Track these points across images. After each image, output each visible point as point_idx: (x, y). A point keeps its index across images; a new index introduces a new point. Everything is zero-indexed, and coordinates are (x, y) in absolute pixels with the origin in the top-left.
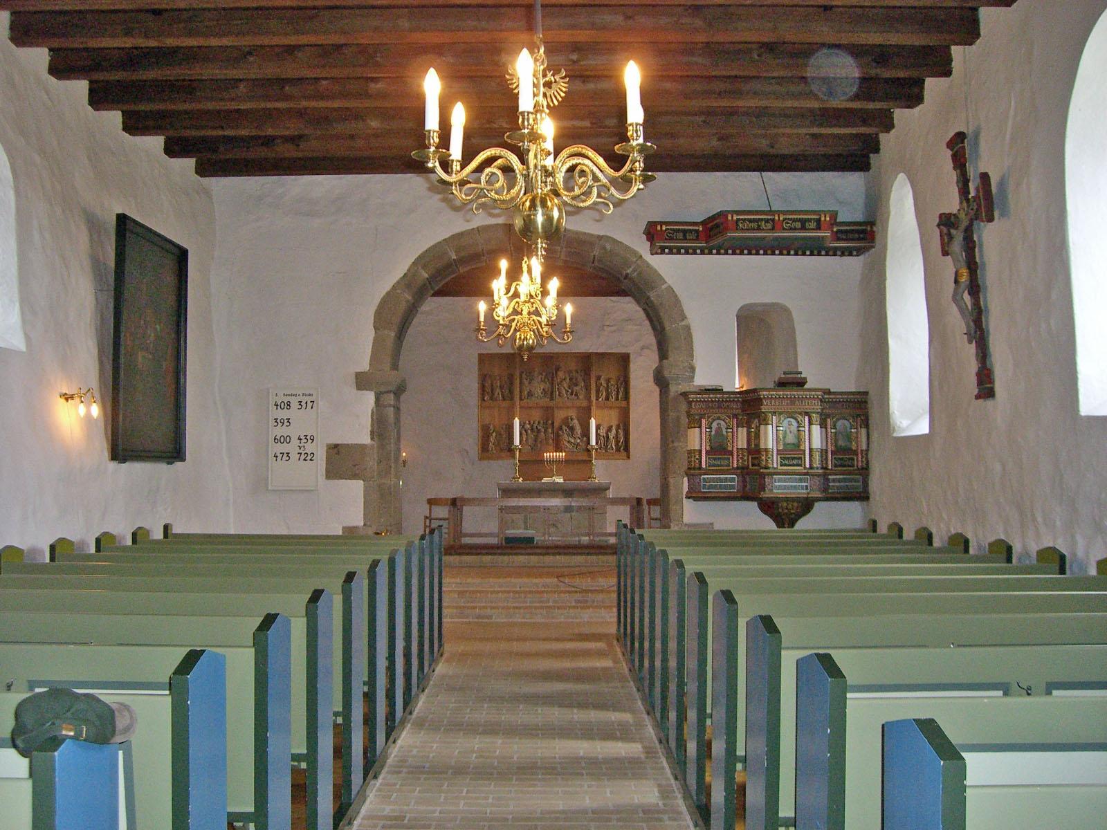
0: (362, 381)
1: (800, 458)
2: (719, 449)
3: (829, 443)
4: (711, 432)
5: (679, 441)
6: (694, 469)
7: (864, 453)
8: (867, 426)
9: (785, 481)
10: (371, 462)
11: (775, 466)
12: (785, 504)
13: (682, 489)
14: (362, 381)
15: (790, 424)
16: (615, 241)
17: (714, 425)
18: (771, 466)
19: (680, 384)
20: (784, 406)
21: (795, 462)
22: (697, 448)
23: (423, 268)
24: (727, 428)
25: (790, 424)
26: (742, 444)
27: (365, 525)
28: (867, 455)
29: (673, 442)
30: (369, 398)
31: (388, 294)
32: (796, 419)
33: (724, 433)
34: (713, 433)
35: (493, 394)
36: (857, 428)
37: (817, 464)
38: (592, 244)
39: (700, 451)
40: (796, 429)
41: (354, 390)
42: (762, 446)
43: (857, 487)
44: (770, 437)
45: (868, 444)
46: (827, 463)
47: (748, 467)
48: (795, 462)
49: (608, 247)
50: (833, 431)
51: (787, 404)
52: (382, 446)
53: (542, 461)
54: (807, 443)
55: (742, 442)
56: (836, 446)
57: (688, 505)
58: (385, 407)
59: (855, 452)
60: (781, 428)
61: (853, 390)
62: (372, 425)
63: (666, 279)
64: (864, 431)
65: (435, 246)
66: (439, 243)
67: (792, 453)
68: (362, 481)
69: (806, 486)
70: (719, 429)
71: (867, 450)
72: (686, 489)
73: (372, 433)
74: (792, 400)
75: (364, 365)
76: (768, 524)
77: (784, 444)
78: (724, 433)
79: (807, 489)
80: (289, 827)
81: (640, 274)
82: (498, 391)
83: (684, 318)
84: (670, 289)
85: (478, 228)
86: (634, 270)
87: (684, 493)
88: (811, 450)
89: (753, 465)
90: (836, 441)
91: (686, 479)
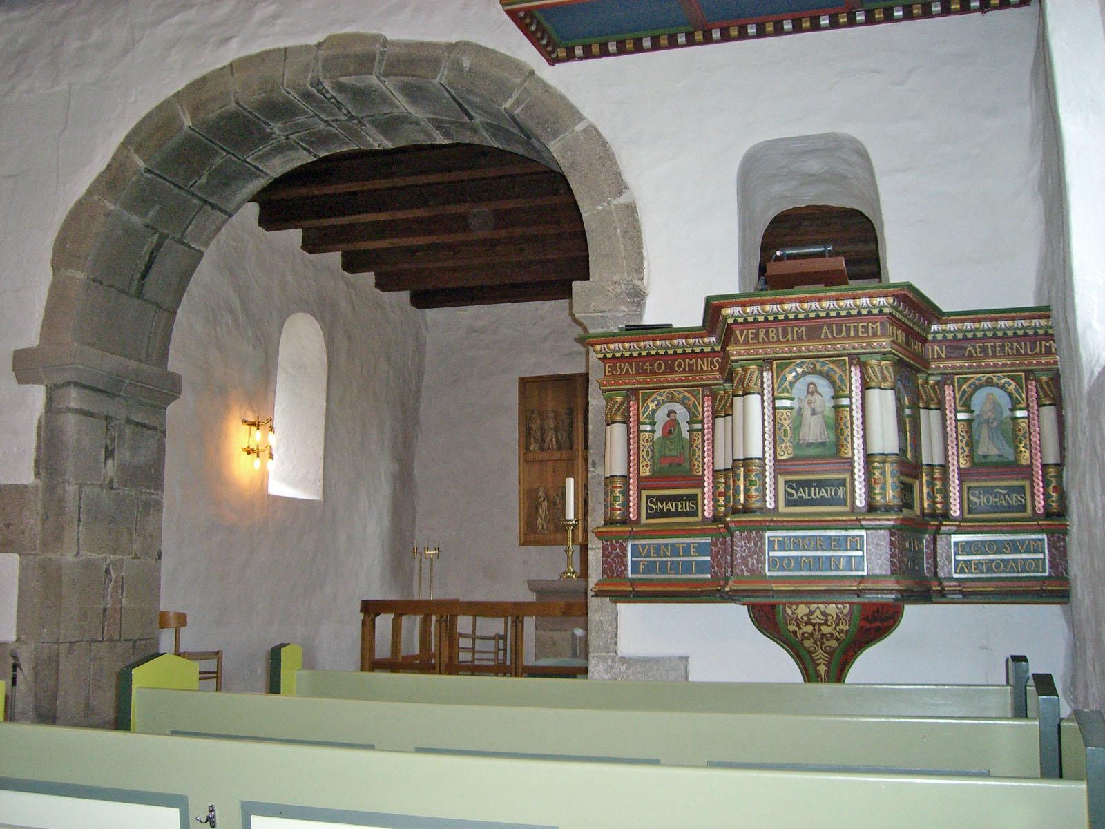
0: (25, 367)
1: (842, 483)
3: (952, 450)
4: (653, 431)
7: (1052, 471)
8: (1058, 402)
9: (798, 544)
10: (32, 520)
14: (25, 367)
15: (812, 391)
16: (478, 49)
18: (755, 503)
23: (137, 151)
25: (812, 391)
27: (18, 640)
28: (1059, 476)
30: (37, 395)
31: (79, 204)
32: (828, 376)
33: (686, 435)
34: (658, 434)
35: (543, 441)
36: (1027, 408)
37: (813, 489)
38: (435, 63)
40: (830, 404)
41: (14, 383)
45: (1062, 448)
46: (946, 502)
49: (466, 63)
50: (961, 416)
51: (800, 339)
52: (50, 489)
54: (858, 442)
56: (971, 456)
58: (60, 412)
59: (1027, 472)
60: (787, 403)
61: (1031, 304)
62: (38, 447)
63: (585, 113)
64: (1048, 413)
65: (159, 109)
66: (166, 103)
67: (813, 473)
68: (17, 556)
70: (671, 426)
71: (1060, 465)
73: (37, 463)
75: (31, 338)
76: (778, 665)
77: (797, 446)
81: (528, 107)
82: (550, 435)
83: (620, 186)
84: (593, 133)
85: (231, 65)
86: (518, 103)
88: (869, 458)
90: (971, 444)
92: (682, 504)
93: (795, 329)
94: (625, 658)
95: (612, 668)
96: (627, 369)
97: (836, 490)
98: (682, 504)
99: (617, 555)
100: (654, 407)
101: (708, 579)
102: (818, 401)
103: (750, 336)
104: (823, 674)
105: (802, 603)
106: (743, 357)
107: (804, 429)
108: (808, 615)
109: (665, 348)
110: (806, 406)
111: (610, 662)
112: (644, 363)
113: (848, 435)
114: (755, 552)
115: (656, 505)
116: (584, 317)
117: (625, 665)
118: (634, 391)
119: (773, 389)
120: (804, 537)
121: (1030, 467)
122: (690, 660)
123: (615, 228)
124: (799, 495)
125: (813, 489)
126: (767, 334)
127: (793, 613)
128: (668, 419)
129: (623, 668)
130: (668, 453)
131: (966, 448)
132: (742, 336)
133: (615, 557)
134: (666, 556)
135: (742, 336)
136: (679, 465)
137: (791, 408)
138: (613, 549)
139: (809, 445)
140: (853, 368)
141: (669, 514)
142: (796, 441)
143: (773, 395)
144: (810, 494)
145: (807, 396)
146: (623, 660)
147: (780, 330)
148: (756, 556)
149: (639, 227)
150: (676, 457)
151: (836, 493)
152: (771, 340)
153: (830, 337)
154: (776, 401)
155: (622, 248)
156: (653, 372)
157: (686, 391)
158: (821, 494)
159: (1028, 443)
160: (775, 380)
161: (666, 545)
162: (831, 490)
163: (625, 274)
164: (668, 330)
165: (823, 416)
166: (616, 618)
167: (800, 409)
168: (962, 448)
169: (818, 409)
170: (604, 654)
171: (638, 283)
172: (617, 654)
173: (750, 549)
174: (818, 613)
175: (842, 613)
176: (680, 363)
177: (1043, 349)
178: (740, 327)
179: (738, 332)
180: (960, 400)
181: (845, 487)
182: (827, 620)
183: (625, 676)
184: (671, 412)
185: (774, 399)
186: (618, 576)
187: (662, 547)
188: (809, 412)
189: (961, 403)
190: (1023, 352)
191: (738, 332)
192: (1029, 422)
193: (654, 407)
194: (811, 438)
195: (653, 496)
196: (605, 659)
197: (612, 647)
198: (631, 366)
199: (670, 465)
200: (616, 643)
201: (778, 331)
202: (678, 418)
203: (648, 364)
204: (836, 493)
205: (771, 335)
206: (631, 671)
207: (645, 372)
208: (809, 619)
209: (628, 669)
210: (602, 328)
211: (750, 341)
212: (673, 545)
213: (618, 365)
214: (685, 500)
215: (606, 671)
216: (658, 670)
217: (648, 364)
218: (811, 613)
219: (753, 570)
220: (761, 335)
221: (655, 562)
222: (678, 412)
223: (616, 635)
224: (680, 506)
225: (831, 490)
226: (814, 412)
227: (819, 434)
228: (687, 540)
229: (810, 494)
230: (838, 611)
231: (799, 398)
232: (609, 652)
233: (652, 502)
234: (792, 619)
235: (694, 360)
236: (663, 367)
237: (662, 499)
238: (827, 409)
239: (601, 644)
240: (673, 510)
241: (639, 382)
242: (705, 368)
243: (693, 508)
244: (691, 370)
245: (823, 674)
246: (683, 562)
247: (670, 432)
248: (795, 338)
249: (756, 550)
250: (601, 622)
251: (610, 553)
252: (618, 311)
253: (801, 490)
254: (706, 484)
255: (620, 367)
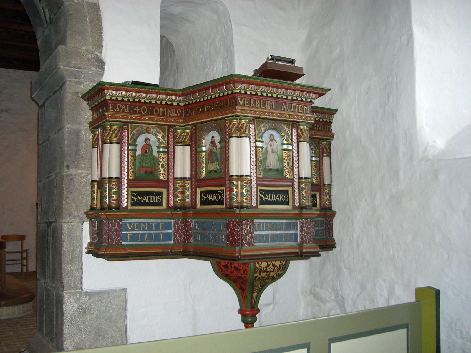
2: (147, 177)
5: (77, 167)
6: (110, 208)
11: (254, 204)
12: (264, 264)
13: (81, 239)
15: (272, 140)
17: (140, 141)
19: (82, 83)
20: (268, 111)
21: (279, 198)
22: (115, 174)
24: (159, 147)
25: (272, 140)
26: (183, 171)
29: (68, 167)
34: (138, 153)
37: (272, 195)
39: (119, 180)
42: (234, 171)
43: (167, 237)
44: (242, 157)
47: (193, 206)
48: (279, 198)
51: (271, 108)
53: (187, 214)
55: (182, 163)
57: (90, 262)
69: (296, 235)
72: (86, 239)
74: (279, 102)
78: (155, 154)
79: (296, 240)
80: (435, 352)
87: (85, 245)
89: (203, 203)
91: (86, 226)
92: (153, 197)
93: (269, 102)
94: (88, 292)
95: (79, 299)
96: (124, 109)
97: (283, 196)
98: (153, 197)
99: (116, 230)
100: (159, 137)
101: (171, 244)
102: (275, 145)
103: (246, 102)
104: (254, 298)
105: (264, 261)
106: (243, 114)
107: (268, 160)
108: (266, 267)
109: (150, 99)
110: (269, 147)
111: (78, 296)
112: (135, 107)
113: (291, 166)
114: (250, 232)
115: (137, 197)
116: (66, 70)
117: (88, 297)
118: (126, 123)
119: (255, 135)
120: (271, 223)
121: (293, 180)
122: (128, 290)
123: (85, 16)
124: (266, 198)
125: (272, 195)
126: (255, 103)
127: (260, 266)
128: (145, 143)
129: (87, 299)
130: (144, 165)
131: (315, 174)
132: (241, 102)
133: (114, 231)
134: (144, 230)
135: (241, 102)
136: (151, 173)
137: (262, 148)
138: (113, 226)
139: (271, 170)
140: (293, 129)
141: (144, 204)
142: (264, 167)
143: (255, 139)
144: (271, 199)
145: (274, 141)
146: (87, 293)
147: (261, 101)
148: (250, 235)
149: (101, 19)
150: (150, 168)
151: (283, 198)
152: (257, 106)
153: (286, 110)
154: (257, 143)
155: (89, 30)
156: (140, 113)
157: (158, 127)
158: (276, 198)
159: (319, 173)
160: (256, 131)
161: (144, 223)
162: (281, 196)
163: (91, 47)
164: (157, 88)
165: (277, 154)
166: (82, 267)
167: (266, 149)
168: (314, 174)
169: (275, 149)
170: (73, 291)
171: (99, 54)
172: (82, 290)
173: (247, 230)
174: (271, 266)
175: (282, 265)
176: (156, 110)
177: (327, 129)
178: (241, 96)
179: (239, 99)
180: (131, 139)
181: (288, 195)
182: (274, 269)
183: (87, 304)
184: (147, 139)
185: (256, 141)
186: (116, 243)
187: (142, 224)
188: (271, 151)
189: (132, 140)
190: (320, 129)
191: (239, 99)
192: (320, 163)
193: (159, 137)
194: (271, 166)
195: (135, 192)
196: (74, 294)
197: (79, 286)
198: (126, 107)
199: (146, 172)
200: (81, 283)
201: (260, 101)
202: (151, 143)
203: (137, 107)
204: (283, 198)
205: (257, 103)
206: (91, 300)
207: (135, 112)
208: (266, 269)
209: (89, 299)
210: (76, 78)
211: (246, 105)
212: (148, 223)
213: (118, 105)
214: (155, 195)
215: (75, 302)
216: (108, 298)
217: (137, 107)
218: (268, 265)
219: (249, 243)
220: (252, 103)
221: (138, 234)
222: (151, 140)
223: (82, 278)
224: (151, 199)
225: (281, 196)
226: (273, 151)
227: (275, 163)
228: (159, 220)
229: (271, 199)
230: (280, 264)
231: (266, 142)
232: (77, 290)
233: (134, 195)
234: (258, 270)
235: (165, 109)
236: (147, 110)
237: (140, 194)
238: (279, 150)
239: (72, 284)
240: (147, 201)
241: (132, 118)
242: (172, 115)
243: (160, 200)
244: (163, 115)
245: (254, 298)
246: (155, 233)
247: (146, 152)
248: (269, 108)
249: (250, 231)
250: (72, 270)
251: (112, 229)
252: (89, 69)
253: (267, 195)
254: (126, 182)
255: (119, 106)
